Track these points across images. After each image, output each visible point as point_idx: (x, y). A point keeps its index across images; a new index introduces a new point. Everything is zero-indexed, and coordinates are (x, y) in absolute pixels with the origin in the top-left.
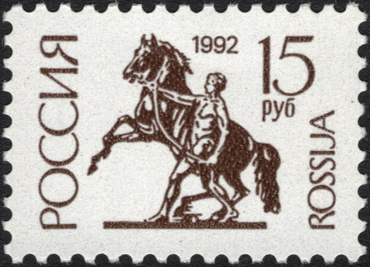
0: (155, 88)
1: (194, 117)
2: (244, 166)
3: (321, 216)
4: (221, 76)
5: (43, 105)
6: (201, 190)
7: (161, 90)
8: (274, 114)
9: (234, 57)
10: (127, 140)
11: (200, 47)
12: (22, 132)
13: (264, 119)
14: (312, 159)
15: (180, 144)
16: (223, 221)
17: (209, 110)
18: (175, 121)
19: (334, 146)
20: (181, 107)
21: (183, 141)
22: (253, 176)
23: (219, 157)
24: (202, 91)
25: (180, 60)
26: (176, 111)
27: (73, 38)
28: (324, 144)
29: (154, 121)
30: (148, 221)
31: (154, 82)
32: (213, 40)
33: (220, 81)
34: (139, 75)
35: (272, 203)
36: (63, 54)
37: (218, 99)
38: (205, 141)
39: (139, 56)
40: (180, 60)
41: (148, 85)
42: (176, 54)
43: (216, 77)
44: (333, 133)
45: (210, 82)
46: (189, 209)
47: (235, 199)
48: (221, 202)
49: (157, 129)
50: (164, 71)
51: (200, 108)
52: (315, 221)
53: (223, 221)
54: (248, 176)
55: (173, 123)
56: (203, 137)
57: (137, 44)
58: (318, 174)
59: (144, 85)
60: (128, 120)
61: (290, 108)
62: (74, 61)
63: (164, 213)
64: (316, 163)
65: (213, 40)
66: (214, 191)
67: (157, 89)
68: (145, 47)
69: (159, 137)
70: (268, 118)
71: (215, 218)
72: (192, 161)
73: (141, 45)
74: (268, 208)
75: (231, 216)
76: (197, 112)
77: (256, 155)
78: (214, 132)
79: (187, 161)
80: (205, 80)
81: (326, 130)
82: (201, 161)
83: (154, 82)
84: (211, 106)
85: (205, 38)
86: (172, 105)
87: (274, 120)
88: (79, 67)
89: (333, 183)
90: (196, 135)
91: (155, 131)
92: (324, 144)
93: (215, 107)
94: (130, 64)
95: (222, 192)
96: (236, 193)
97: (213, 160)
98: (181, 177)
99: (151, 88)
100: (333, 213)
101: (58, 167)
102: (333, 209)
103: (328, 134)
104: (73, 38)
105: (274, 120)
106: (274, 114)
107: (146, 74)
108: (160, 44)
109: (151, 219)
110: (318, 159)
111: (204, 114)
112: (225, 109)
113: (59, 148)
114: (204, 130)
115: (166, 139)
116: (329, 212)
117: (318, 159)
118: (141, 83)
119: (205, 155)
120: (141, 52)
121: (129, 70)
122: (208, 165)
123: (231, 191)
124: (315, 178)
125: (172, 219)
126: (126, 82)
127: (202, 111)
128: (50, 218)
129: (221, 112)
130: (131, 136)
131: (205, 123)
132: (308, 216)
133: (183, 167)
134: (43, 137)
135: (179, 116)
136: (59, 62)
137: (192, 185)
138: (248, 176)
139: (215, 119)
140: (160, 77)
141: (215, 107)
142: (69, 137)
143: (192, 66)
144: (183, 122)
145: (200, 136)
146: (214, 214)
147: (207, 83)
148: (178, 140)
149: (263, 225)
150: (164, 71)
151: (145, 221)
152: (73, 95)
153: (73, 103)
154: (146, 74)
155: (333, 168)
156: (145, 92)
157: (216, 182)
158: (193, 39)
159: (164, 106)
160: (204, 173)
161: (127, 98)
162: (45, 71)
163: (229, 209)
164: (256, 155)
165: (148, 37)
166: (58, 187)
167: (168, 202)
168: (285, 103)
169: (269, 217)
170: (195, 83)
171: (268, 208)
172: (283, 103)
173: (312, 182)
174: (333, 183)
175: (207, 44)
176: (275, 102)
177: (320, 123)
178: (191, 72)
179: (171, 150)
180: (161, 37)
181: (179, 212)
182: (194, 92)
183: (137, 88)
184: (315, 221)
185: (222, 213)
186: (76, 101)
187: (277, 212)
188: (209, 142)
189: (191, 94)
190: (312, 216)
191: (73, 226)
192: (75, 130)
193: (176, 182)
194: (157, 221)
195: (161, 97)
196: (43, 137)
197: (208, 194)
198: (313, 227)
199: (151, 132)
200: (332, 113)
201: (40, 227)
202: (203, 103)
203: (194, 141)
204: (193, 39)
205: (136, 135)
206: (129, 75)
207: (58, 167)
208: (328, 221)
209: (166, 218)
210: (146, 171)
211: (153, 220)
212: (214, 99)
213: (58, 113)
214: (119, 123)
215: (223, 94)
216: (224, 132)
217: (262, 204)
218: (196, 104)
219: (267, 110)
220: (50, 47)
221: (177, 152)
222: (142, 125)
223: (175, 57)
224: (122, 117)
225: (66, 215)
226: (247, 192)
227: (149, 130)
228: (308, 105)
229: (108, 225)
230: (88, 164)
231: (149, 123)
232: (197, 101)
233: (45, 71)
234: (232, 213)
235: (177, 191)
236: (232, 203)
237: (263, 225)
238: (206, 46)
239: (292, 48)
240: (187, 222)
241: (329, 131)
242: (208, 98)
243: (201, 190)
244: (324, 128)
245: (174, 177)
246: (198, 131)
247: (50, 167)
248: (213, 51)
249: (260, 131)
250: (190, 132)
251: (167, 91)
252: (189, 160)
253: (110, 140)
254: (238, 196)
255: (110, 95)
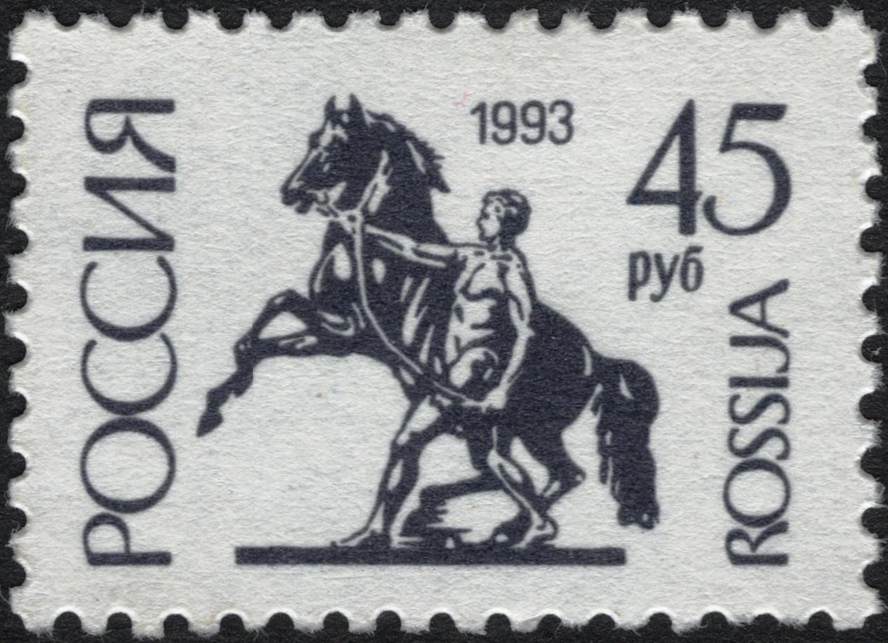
0: (358, 225)
1: (452, 298)
2: (569, 418)
3: (754, 533)
4: (518, 200)
5: (91, 267)
6: (467, 471)
7: (372, 230)
8: (654, 285)
9: (562, 151)
10: (291, 351)
11: (491, 128)
12: (46, 329)
13: (632, 296)
14: (734, 399)
15: (418, 363)
16: (522, 545)
17: (487, 278)
18: (407, 304)
19: (785, 368)
20: (418, 271)
21: (423, 357)
22: (593, 438)
23: (511, 395)
24: (472, 235)
25: (418, 160)
26: (408, 283)
27: (165, 107)
28: (764, 362)
29: (354, 306)
30: (339, 544)
31: (357, 212)
32: (519, 112)
33: (514, 210)
34: (320, 195)
35: (638, 503)
36: (141, 146)
37: (509, 252)
38: (477, 354)
39: (320, 149)
40: (418, 160)
41: (343, 218)
42: (410, 145)
43: (505, 201)
44: (785, 333)
45: (490, 209)
46: (440, 516)
47: (549, 493)
48: (514, 498)
49: (362, 325)
50: (379, 188)
51: (465, 276)
52: (740, 547)
53: (522, 545)
54: (582, 439)
55: (402, 310)
56: (474, 344)
57: (315, 120)
58: (747, 435)
59: (331, 218)
60: (289, 302)
61: (692, 267)
62: (166, 162)
63: (377, 525)
64: (743, 409)
65: (519, 112)
66: (497, 471)
67: (363, 230)
68: (334, 127)
69: (363, 344)
70: (644, 292)
71: (502, 538)
72: (446, 402)
73: (325, 124)
74: (625, 518)
75: (539, 533)
76: (460, 284)
77: (599, 389)
78: (499, 331)
79: (433, 403)
80: (480, 206)
81: (770, 328)
82: (469, 403)
83: (357, 212)
84: (492, 266)
85: (497, 107)
86: (398, 267)
87: (656, 298)
88: (178, 177)
89: (784, 455)
90: (457, 340)
91: (357, 328)
92: (764, 362)
93: (503, 273)
94: (299, 168)
95: (517, 477)
96: (551, 481)
97: (497, 399)
98: (422, 439)
99: (348, 226)
100: (782, 528)
101: (127, 417)
102: (784, 517)
103: (774, 339)
104: (165, 107)
105: (656, 298)
106: (654, 285)
107: (336, 193)
108: (369, 120)
109: (345, 541)
110: (749, 398)
111: (475, 288)
112: (528, 279)
113: (129, 372)
114: (475, 327)
115: (383, 346)
116: (773, 524)
117: (749, 398)
118: (325, 214)
119: (478, 386)
120: (325, 140)
121: (295, 185)
122: (484, 410)
123: (539, 475)
124: (743, 441)
125: (397, 540)
126: (290, 211)
127: (468, 283)
128: (107, 539)
129: (515, 283)
130: (302, 341)
131: (478, 311)
132: (742, 502)
133: (427, 414)
134: (90, 347)
135: (415, 296)
136: (128, 163)
137: (446, 460)
138: (582, 439)
139: (502, 299)
140: (369, 200)
141: (503, 273)
142: (152, 347)
143: (448, 175)
144: (425, 309)
145: (463, 343)
146: (498, 531)
147: (484, 215)
148: (413, 351)
149: (614, 557)
150: (379, 188)
151: (333, 544)
152: (161, 242)
153: (163, 263)
154: (336, 193)
155: (785, 421)
156: (335, 236)
157: (505, 452)
158: (473, 112)
159: (379, 268)
160: (478, 431)
161: (292, 250)
162: (99, 187)
163: (536, 518)
164: (599, 389)
165: (342, 104)
166: (127, 465)
167: (389, 499)
168: (682, 257)
169: (630, 538)
170: (457, 213)
171: (625, 518)
172: (676, 258)
173: (737, 452)
174: (784, 455)
175: (503, 121)
176: (658, 257)
177: (753, 311)
178: (444, 188)
179: (396, 374)
180: (372, 104)
181: (411, 526)
182: (453, 236)
183: (315, 225)
184: (740, 547)
185: (516, 528)
186: (169, 256)
187: (648, 526)
188: (486, 354)
189: (442, 240)
190: (733, 536)
191: (163, 559)
192: (169, 328)
193: (406, 453)
194: (363, 545)
195: (372, 248)
196: (90, 347)
197: (486, 482)
198: (737, 560)
199: (350, 332)
200: (781, 287)
201: (82, 555)
202: (473, 263)
203: (451, 351)
204: (473, 112)
205: (311, 340)
206: (298, 195)
207: (127, 417)
208: (773, 546)
209: (385, 536)
210: (333, 430)
211: (354, 543)
212: (498, 252)
213: (128, 288)
214: (271, 311)
215: (522, 241)
216: (525, 334)
217: (613, 506)
218: (456, 265)
219: (640, 276)
220: (108, 125)
221: (409, 380)
222: (330, 316)
223: (408, 154)
224: (279, 295)
225: (146, 531)
226: (579, 478)
227: (345, 327)
228: (733, 267)
229: (248, 556)
230: (199, 406)
231: (344, 312)
232: (460, 258)
233: (99, 187)
234: (541, 528)
235: (411, 474)
236: (543, 504)
237: (614, 557)
238: (502, 127)
239: (746, 131)
240: (434, 546)
241: (777, 330)
242: (485, 251)
243: (467, 471)
244: (761, 323)
245: (404, 438)
246: (461, 330)
247: (104, 417)
248: (518, 140)
249: (613, 325)
250: (442, 329)
251: (389, 235)
252: (439, 397)
253: (253, 350)
254: (556, 486)
255: (251, 241)
